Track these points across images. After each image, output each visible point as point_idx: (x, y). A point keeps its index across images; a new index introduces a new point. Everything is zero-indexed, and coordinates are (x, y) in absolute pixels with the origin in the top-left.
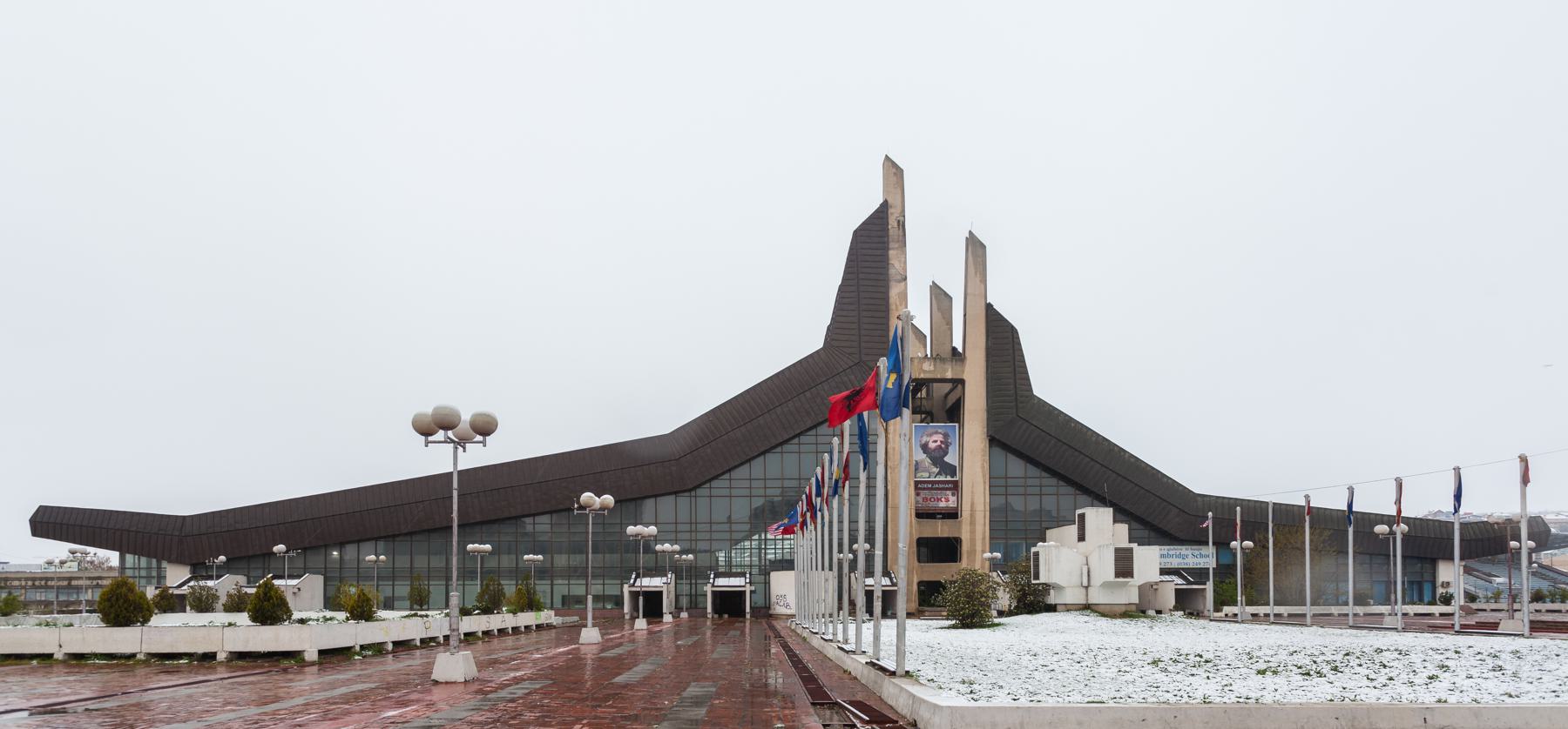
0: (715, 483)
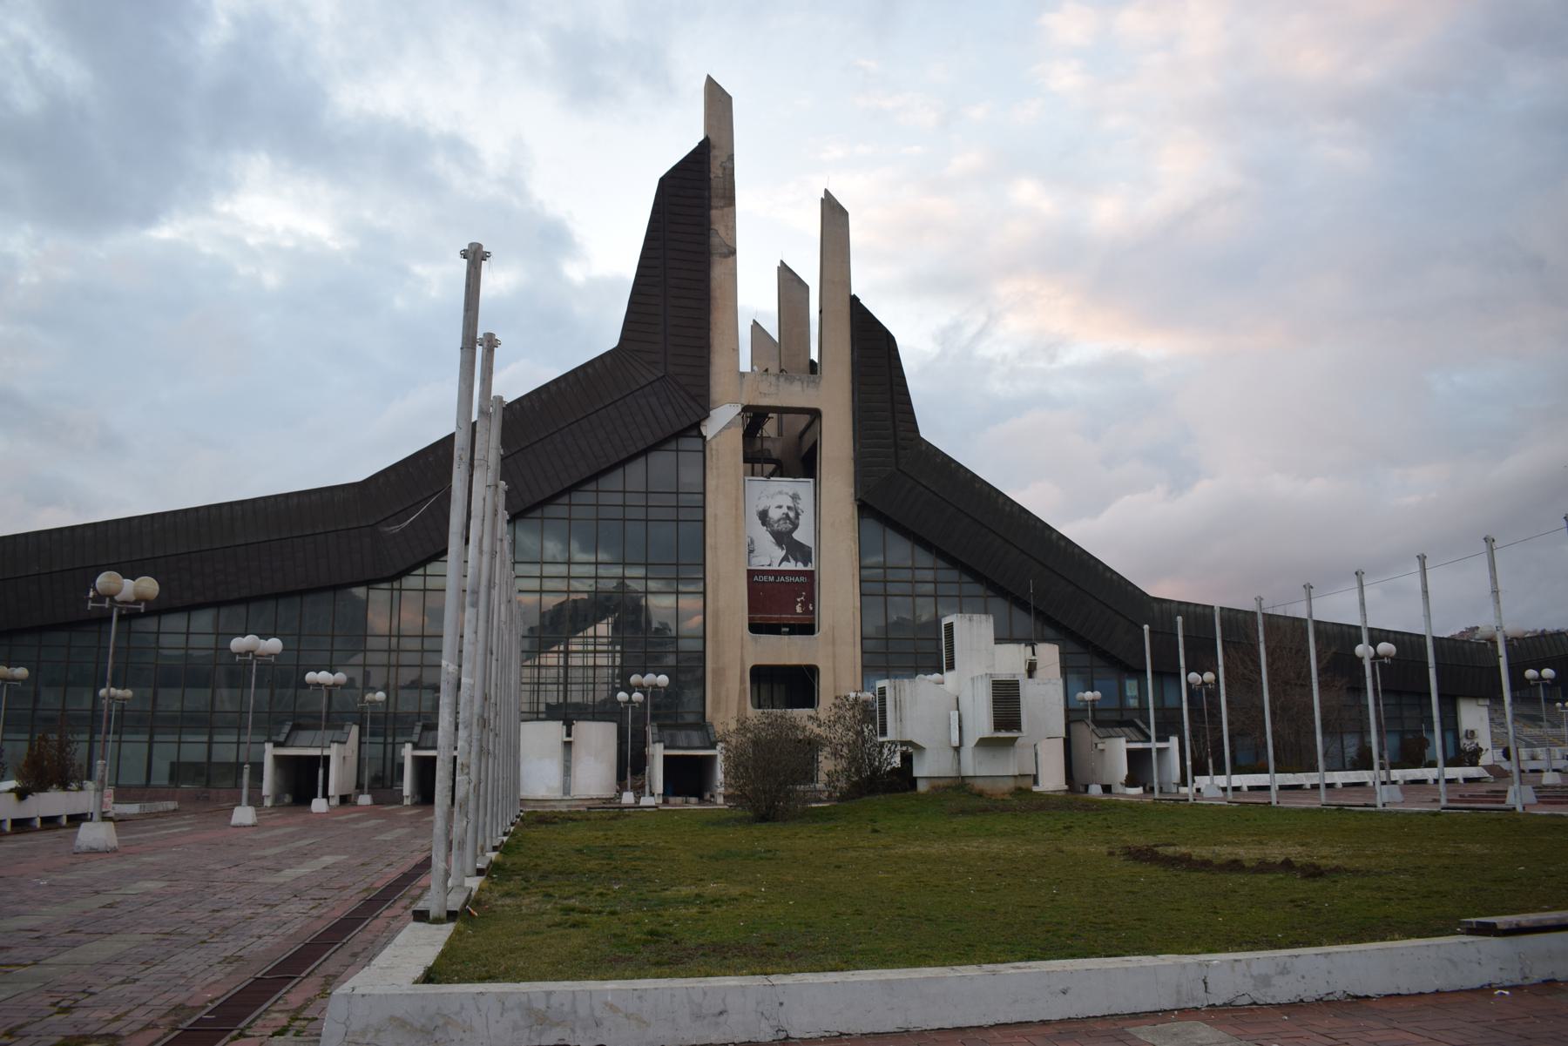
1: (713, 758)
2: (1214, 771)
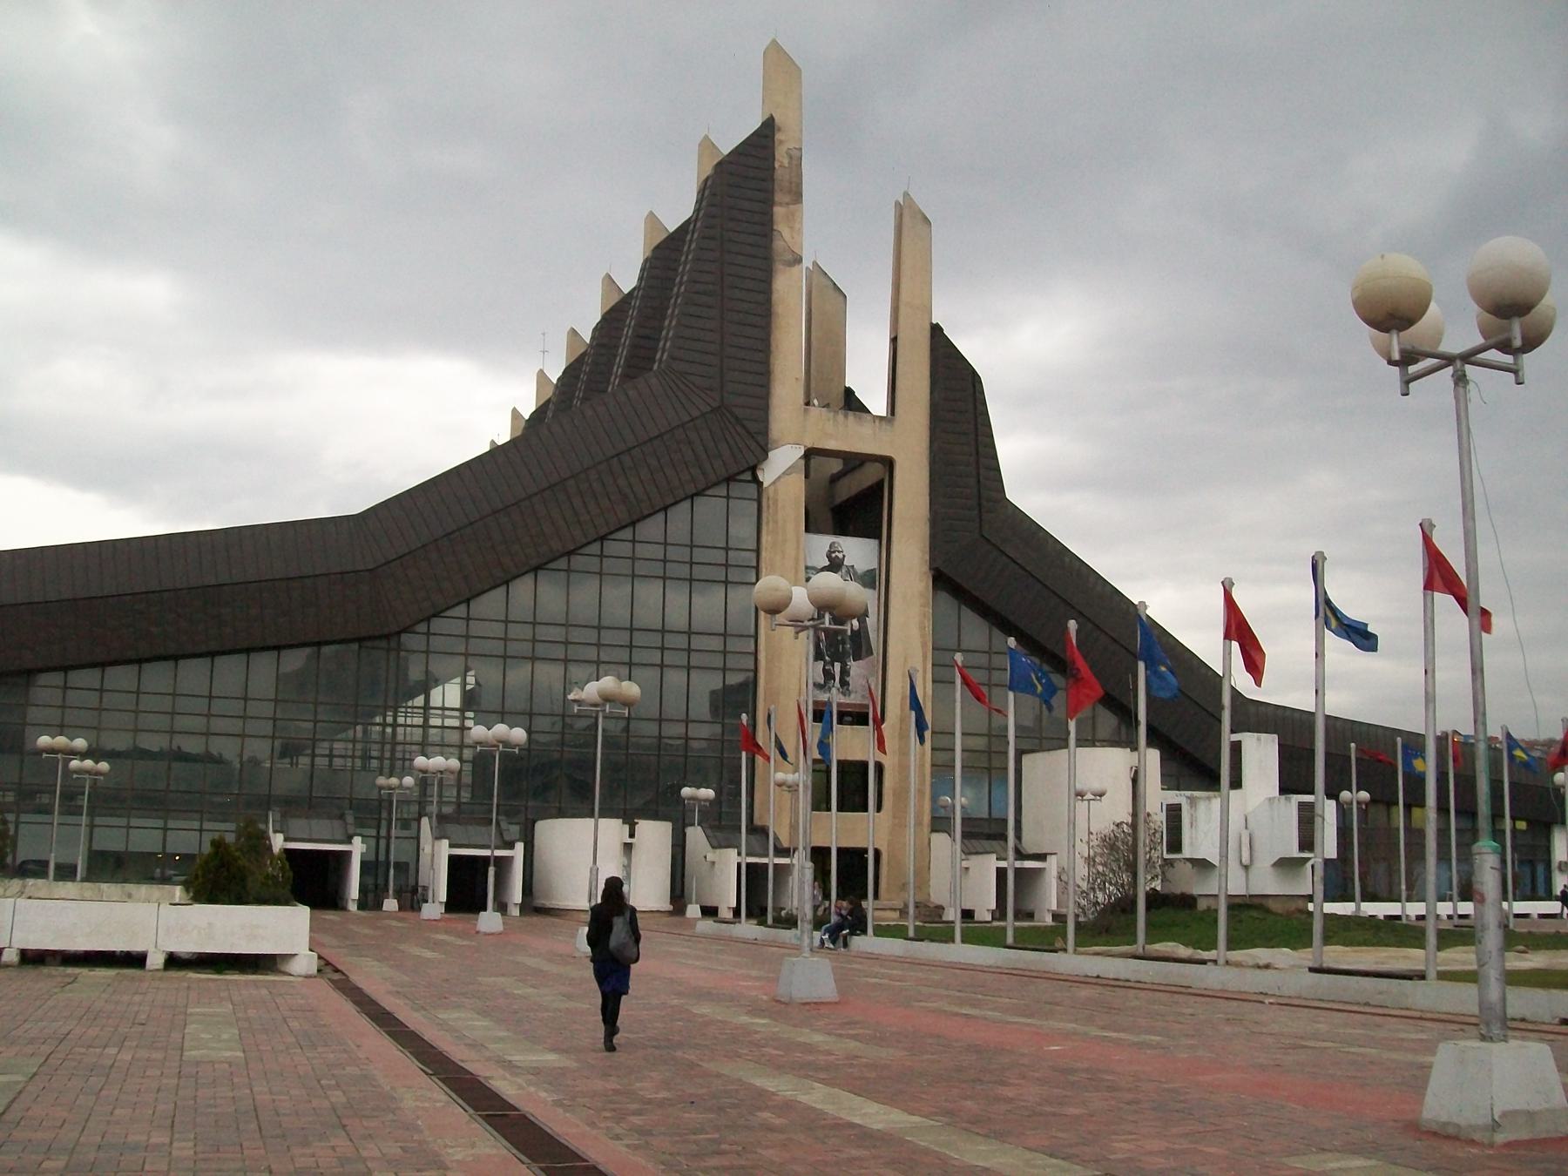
0: (437, 625)
1: (348, 854)
2: (55, 875)
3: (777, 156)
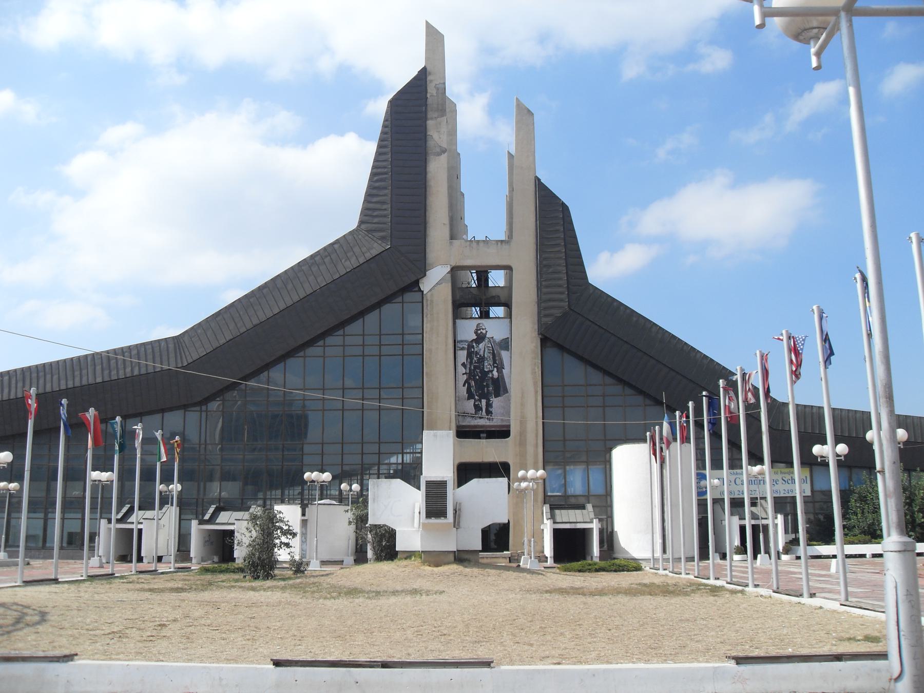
3: (429, 90)
